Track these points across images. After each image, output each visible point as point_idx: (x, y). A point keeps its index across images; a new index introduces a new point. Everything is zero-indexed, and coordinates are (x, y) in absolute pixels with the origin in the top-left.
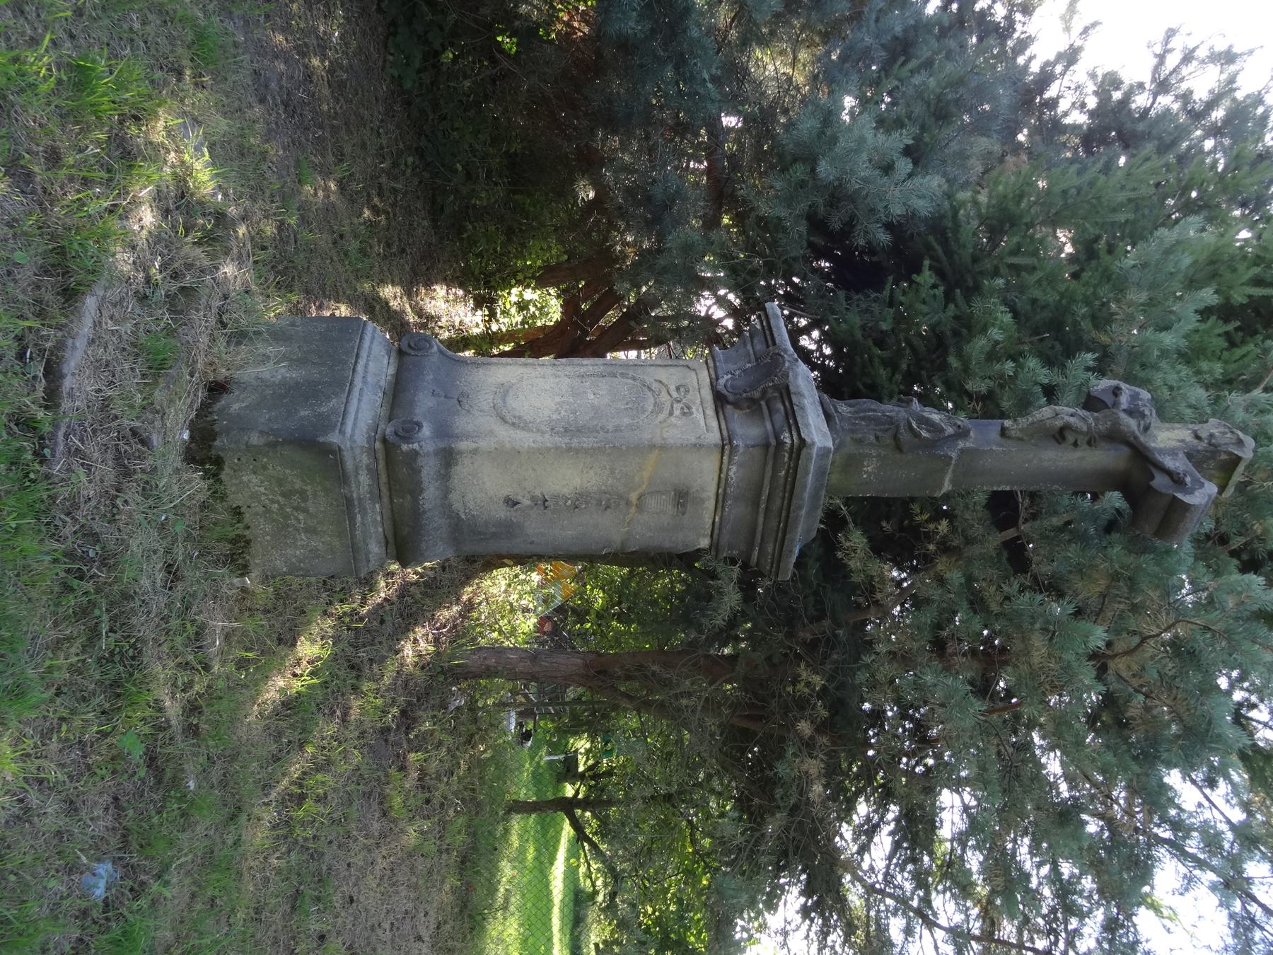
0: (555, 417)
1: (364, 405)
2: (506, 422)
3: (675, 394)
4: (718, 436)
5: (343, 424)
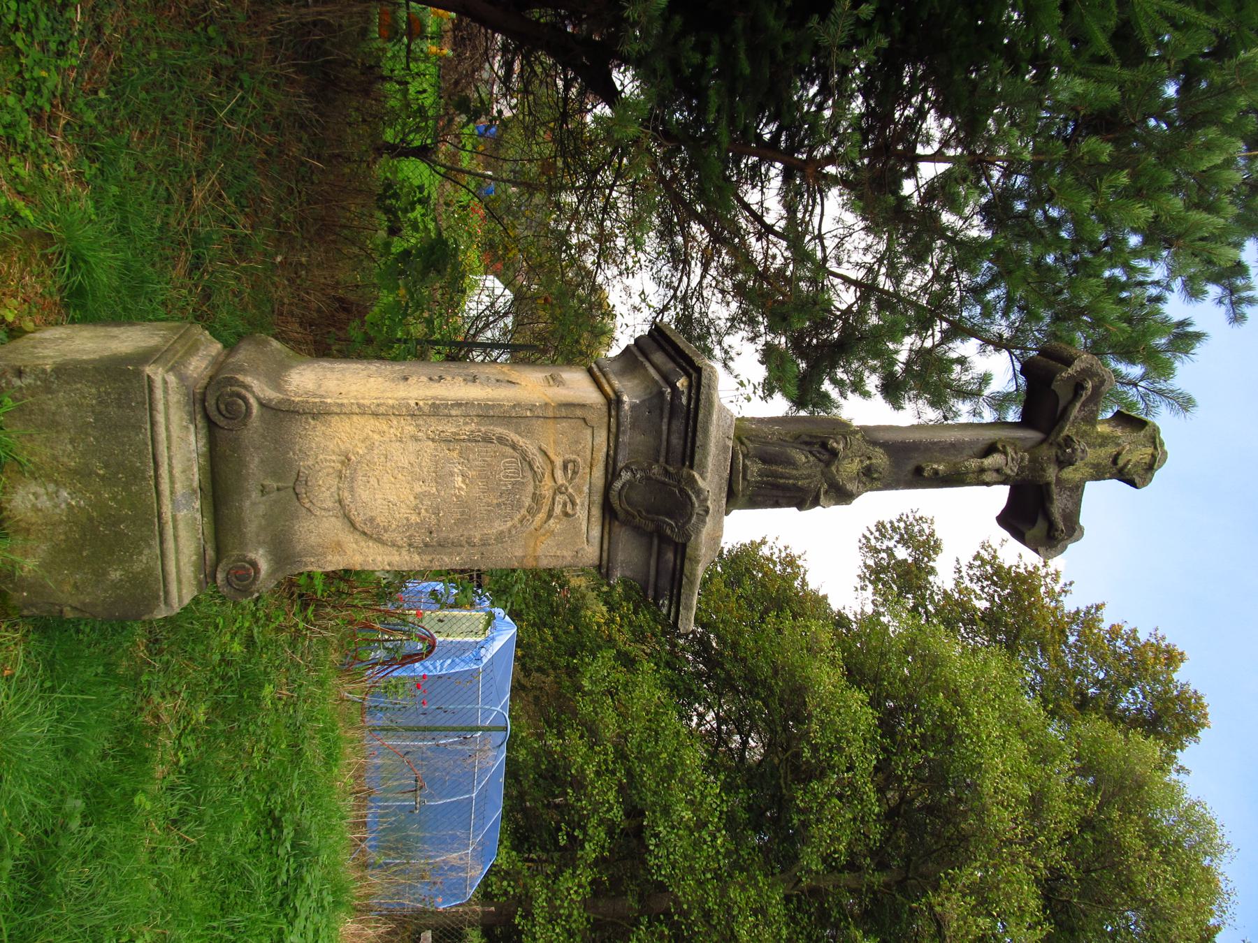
0: (414, 518)
1: (183, 533)
2: (355, 528)
3: (561, 479)
4: (597, 553)
5: (167, 593)
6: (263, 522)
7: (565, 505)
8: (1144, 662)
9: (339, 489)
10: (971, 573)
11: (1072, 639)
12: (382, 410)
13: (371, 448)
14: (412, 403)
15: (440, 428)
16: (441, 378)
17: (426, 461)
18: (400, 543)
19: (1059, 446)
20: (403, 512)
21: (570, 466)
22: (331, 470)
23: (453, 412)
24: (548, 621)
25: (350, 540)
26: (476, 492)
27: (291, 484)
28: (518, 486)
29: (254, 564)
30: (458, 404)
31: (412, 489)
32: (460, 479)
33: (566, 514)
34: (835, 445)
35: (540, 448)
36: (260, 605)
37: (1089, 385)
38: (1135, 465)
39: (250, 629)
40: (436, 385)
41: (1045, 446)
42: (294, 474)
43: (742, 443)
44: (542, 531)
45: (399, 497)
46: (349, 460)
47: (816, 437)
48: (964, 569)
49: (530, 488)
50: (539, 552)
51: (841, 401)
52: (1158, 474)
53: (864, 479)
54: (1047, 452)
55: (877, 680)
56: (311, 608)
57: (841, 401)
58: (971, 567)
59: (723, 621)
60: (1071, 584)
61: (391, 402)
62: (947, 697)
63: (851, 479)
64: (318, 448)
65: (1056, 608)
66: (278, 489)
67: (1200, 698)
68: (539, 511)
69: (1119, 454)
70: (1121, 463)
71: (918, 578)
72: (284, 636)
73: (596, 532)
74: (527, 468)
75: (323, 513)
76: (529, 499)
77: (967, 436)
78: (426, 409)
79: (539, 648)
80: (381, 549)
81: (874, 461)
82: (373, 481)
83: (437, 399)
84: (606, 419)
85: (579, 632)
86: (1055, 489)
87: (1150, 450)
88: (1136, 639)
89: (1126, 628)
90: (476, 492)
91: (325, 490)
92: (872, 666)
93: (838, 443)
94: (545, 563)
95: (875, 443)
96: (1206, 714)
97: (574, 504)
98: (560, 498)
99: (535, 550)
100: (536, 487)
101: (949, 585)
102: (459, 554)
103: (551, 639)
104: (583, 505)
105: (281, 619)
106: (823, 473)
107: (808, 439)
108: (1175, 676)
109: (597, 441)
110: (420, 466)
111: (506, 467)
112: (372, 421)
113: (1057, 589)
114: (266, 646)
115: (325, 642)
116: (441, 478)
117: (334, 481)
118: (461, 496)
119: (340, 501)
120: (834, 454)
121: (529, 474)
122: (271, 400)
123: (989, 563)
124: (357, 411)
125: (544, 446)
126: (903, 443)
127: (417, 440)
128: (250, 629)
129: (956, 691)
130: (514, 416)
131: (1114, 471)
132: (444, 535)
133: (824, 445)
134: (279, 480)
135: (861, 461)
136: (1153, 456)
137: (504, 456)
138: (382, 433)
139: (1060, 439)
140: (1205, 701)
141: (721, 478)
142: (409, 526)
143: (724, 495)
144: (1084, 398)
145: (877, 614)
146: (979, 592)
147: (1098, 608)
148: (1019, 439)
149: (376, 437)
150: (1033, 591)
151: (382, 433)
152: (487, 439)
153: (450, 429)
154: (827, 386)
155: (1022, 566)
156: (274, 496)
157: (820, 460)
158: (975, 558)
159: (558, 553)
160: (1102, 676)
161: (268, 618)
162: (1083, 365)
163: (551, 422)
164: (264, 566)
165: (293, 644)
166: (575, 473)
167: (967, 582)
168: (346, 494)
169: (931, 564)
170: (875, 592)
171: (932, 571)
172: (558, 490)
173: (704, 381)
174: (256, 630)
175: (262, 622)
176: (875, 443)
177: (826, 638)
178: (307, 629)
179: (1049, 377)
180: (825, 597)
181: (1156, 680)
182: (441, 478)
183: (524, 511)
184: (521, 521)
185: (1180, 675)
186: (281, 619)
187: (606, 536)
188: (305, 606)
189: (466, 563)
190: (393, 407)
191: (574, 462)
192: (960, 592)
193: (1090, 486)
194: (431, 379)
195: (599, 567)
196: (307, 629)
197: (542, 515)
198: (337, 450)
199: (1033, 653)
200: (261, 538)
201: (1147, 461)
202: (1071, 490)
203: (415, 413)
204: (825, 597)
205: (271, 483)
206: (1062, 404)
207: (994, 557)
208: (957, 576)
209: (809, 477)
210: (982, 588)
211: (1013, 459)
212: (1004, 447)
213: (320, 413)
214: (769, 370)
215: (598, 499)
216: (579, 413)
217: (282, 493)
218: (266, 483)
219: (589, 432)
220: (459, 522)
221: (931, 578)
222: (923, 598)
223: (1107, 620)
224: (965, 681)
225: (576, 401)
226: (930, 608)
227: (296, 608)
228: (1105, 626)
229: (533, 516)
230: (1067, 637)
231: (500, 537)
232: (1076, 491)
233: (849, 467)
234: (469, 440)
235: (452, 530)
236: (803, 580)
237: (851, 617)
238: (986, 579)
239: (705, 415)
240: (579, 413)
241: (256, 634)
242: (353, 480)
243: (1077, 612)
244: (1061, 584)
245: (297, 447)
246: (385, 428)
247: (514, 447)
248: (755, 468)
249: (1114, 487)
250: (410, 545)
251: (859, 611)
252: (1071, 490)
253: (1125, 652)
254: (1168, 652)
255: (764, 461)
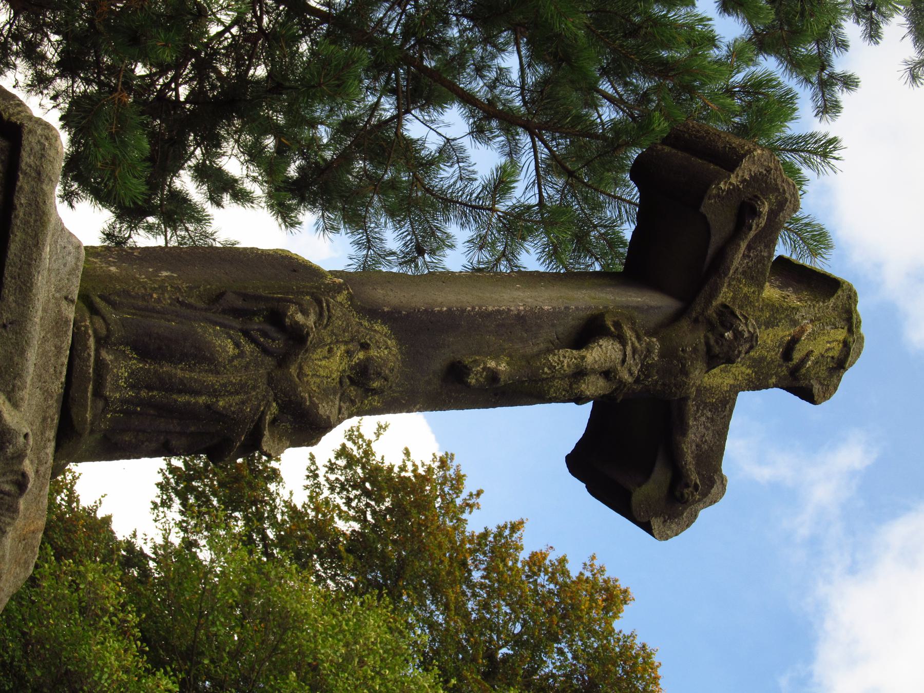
8: (575, 607)
10: (332, 477)
11: (477, 576)
19: (711, 326)
34: (299, 317)
37: (765, 209)
38: (816, 363)
41: (685, 324)
43: (94, 310)
47: (258, 298)
48: (322, 472)
51: (210, 209)
52: (849, 377)
53: (353, 391)
54: (691, 338)
55: (191, 655)
57: (210, 209)
58: (332, 468)
60: (479, 494)
62: (301, 678)
63: (326, 393)
65: (455, 528)
67: (649, 656)
69: (795, 340)
70: (797, 356)
71: (253, 488)
77: (546, 300)
81: (373, 353)
86: (691, 406)
87: (841, 334)
88: (565, 573)
89: (553, 557)
92: (184, 634)
93: (305, 313)
95: (373, 312)
96: (656, 678)
101: (300, 499)
106: (271, 381)
107: (239, 303)
108: (617, 625)
113: (459, 502)
120: (297, 339)
123: (358, 461)
126: (429, 312)
129: (315, 668)
131: (784, 371)
133: (276, 318)
135: (349, 353)
136: (846, 344)
139: (711, 312)
140: (656, 659)
141: (47, 394)
143: (51, 434)
144: (752, 234)
145: (189, 544)
146: (344, 508)
147: (515, 528)
148: (637, 308)
150: (424, 504)
154: (185, 182)
155: (410, 467)
157: (265, 351)
158: (338, 455)
160: (518, 628)
162: (754, 169)
167: (326, 493)
169: (273, 464)
170: (186, 508)
171: (275, 476)
173: (27, 159)
176: (373, 312)
177: (111, 591)
179: (697, 191)
180: (107, 520)
181: (592, 632)
185: (623, 624)
192: (317, 509)
193: (745, 399)
199: (421, 599)
201: (835, 353)
202: (714, 407)
204: (107, 520)
206: (715, 241)
207: (368, 453)
208: (309, 482)
209: (241, 388)
210: (349, 501)
211: (634, 351)
212: (617, 325)
214: (404, 138)
221: (272, 487)
222: (261, 519)
223: (530, 543)
224: (330, 652)
226: (271, 534)
228: (524, 555)
230: (469, 572)
232: (722, 408)
233: (326, 365)
236: (71, 492)
237: (148, 551)
238: (355, 487)
239: (24, 246)
243: (485, 535)
244: (464, 495)
248: (122, 369)
249: (778, 399)
251: (160, 541)
252: (714, 407)
253: (550, 592)
254: (607, 590)
255: (144, 353)
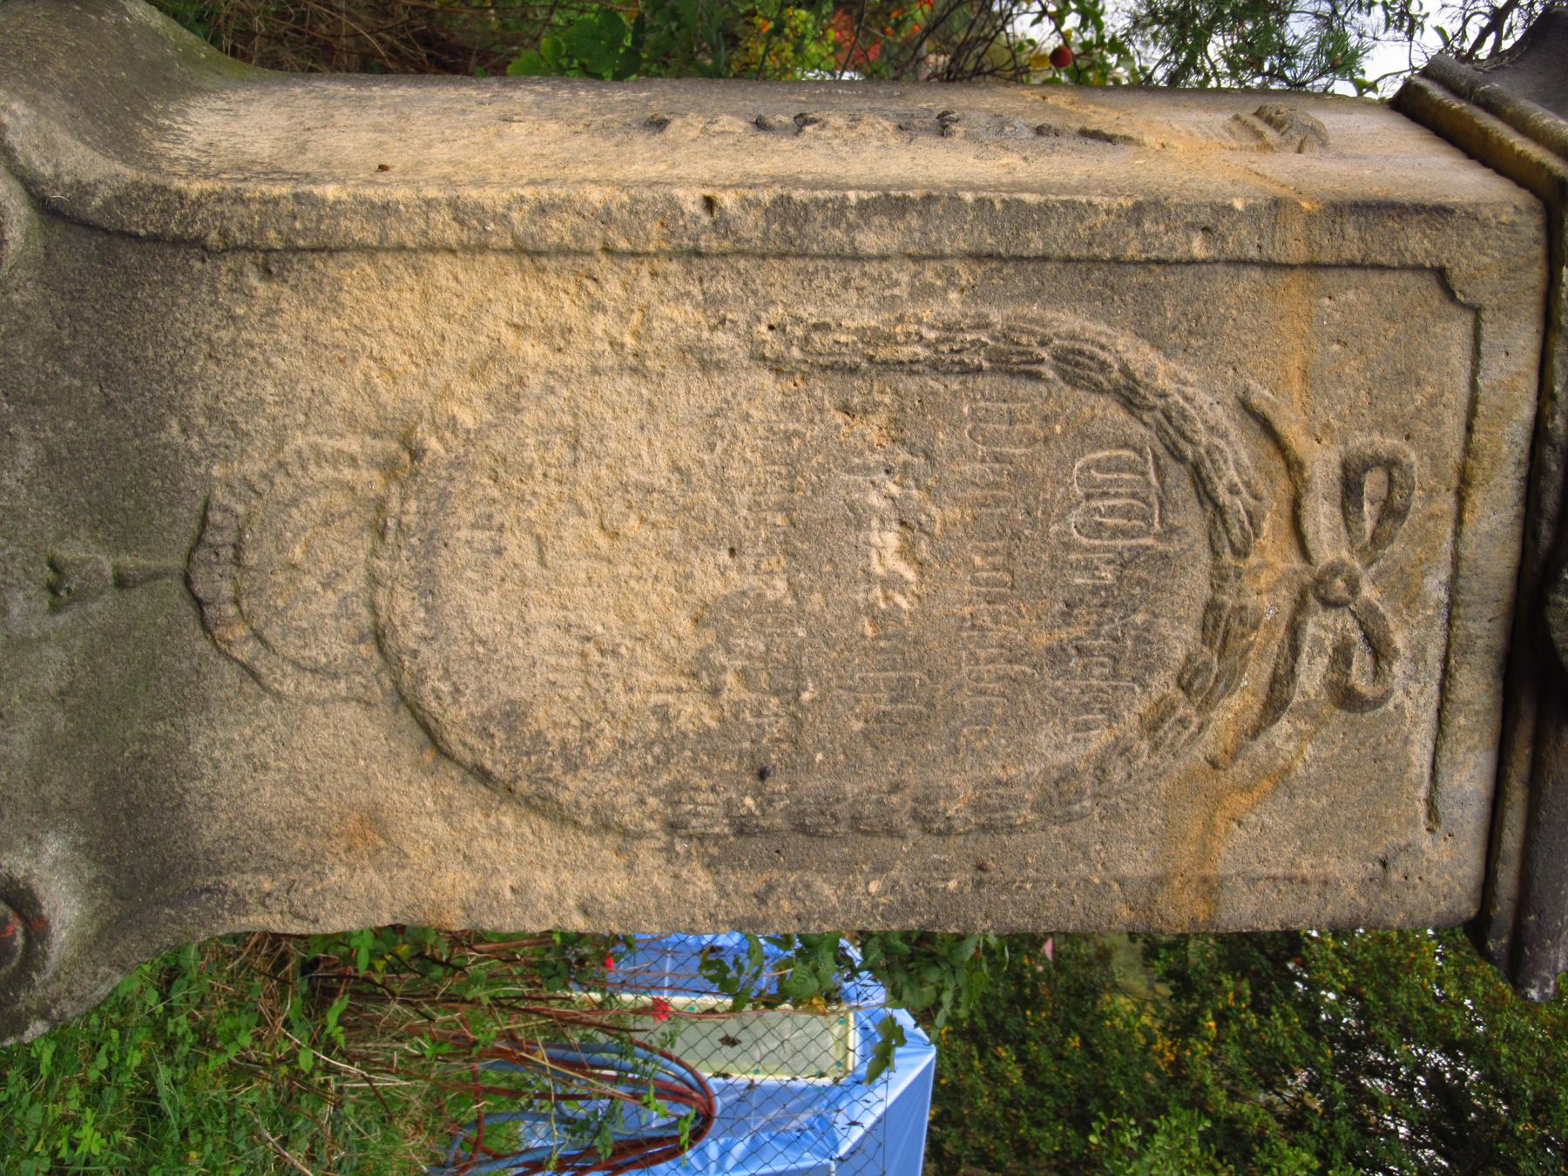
0: (692, 711)
2: (444, 753)
6: (61, 723)
7: (1342, 655)
9: (374, 580)
12: (558, 230)
13: (509, 402)
14: (690, 199)
15: (810, 312)
16: (802, 121)
17: (748, 462)
18: (631, 817)
20: (649, 681)
21: (1373, 483)
22: (341, 501)
23: (869, 241)
24: (1011, 1024)
25: (417, 801)
26: (960, 598)
27: (176, 562)
28: (1143, 571)
29: (22, 900)
30: (891, 204)
31: (683, 582)
32: (892, 539)
33: (1347, 698)
35: (1245, 406)
36: (177, 996)
39: (146, 1072)
40: (785, 144)
42: (186, 514)
44: (1241, 770)
45: (627, 617)
46: (416, 454)
49: (1195, 583)
50: (1224, 863)
56: (339, 1005)
59: (1510, 1037)
61: (596, 196)
64: (285, 401)
66: (121, 582)
68: (1229, 681)
72: (251, 1096)
73: (1469, 777)
74: (1183, 490)
75: (309, 685)
76: (1190, 632)
78: (750, 226)
79: (983, 1103)
80: (552, 841)
82: (518, 547)
83: (796, 182)
84: (1535, 276)
85: (1095, 1057)
90: (960, 598)
91: (315, 585)
94: (1246, 910)
97: (1380, 651)
98: (1321, 628)
99: (1205, 854)
100: (1219, 578)
102: (880, 869)
103: (1015, 1074)
104: (1418, 657)
105: (245, 1040)
109: (1495, 370)
110: (721, 482)
111: (1090, 478)
112: (515, 283)
114: (198, 1123)
115: (385, 1108)
116: (811, 534)
117: (349, 549)
118: (894, 613)
119: (378, 637)
121: (1192, 520)
122: (83, 190)
124: (452, 235)
125: (1261, 395)
127: (708, 363)
128: (146, 1072)
130: (1122, 259)
132: (815, 784)
134: (123, 541)
137: (1086, 437)
138: (558, 335)
142: (670, 745)
149: (532, 351)
151: (558, 335)
152: (1014, 363)
153: (854, 316)
156: (103, 608)
159: (1306, 866)
161: (206, 1038)
163: (1293, 284)
164: (66, 910)
165: (283, 1114)
166: (1391, 512)
168: (404, 604)
172: (1318, 592)
174: (164, 1075)
175: (183, 1050)
178: (328, 1069)
182: (811, 534)
183: (1162, 684)
184: (1152, 726)
186: (245, 1040)
187: (1517, 796)
188: (320, 998)
189: (910, 907)
190: (605, 217)
191: (1390, 464)
194: (761, 125)
195: (1477, 928)
196: (328, 1069)
197: (1241, 702)
198: (364, 410)
200: (54, 791)
203: (699, 245)
205: (92, 556)
213: (292, 245)
215: (1484, 627)
216: (1418, 243)
217: (140, 600)
218: (70, 552)
219: (1458, 330)
220: (880, 728)
225: (1398, 195)
227: (291, 1007)
229: (1206, 706)
231: (1058, 797)
234: (934, 366)
235: (855, 763)
240: (1418, 243)
241: (164, 1090)
242: (432, 542)
245: (199, 398)
246: (572, 312)
247: (1130, 396)
250: (673, 827)
